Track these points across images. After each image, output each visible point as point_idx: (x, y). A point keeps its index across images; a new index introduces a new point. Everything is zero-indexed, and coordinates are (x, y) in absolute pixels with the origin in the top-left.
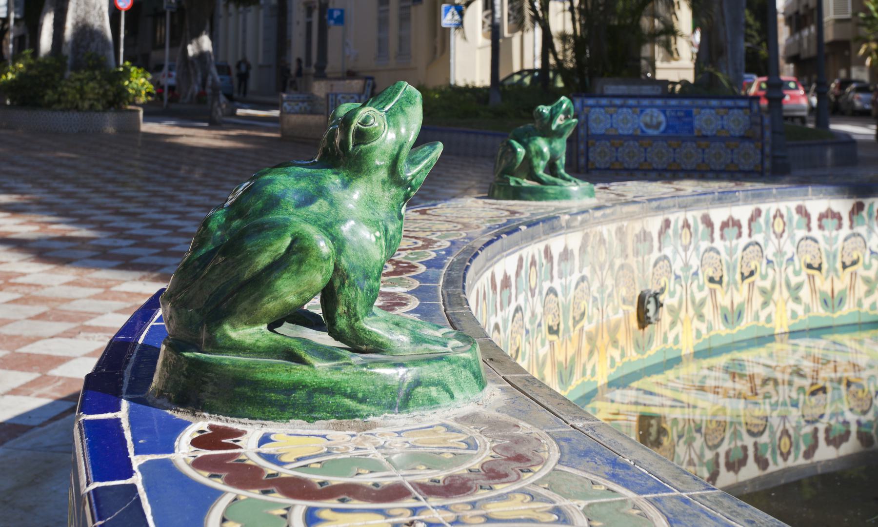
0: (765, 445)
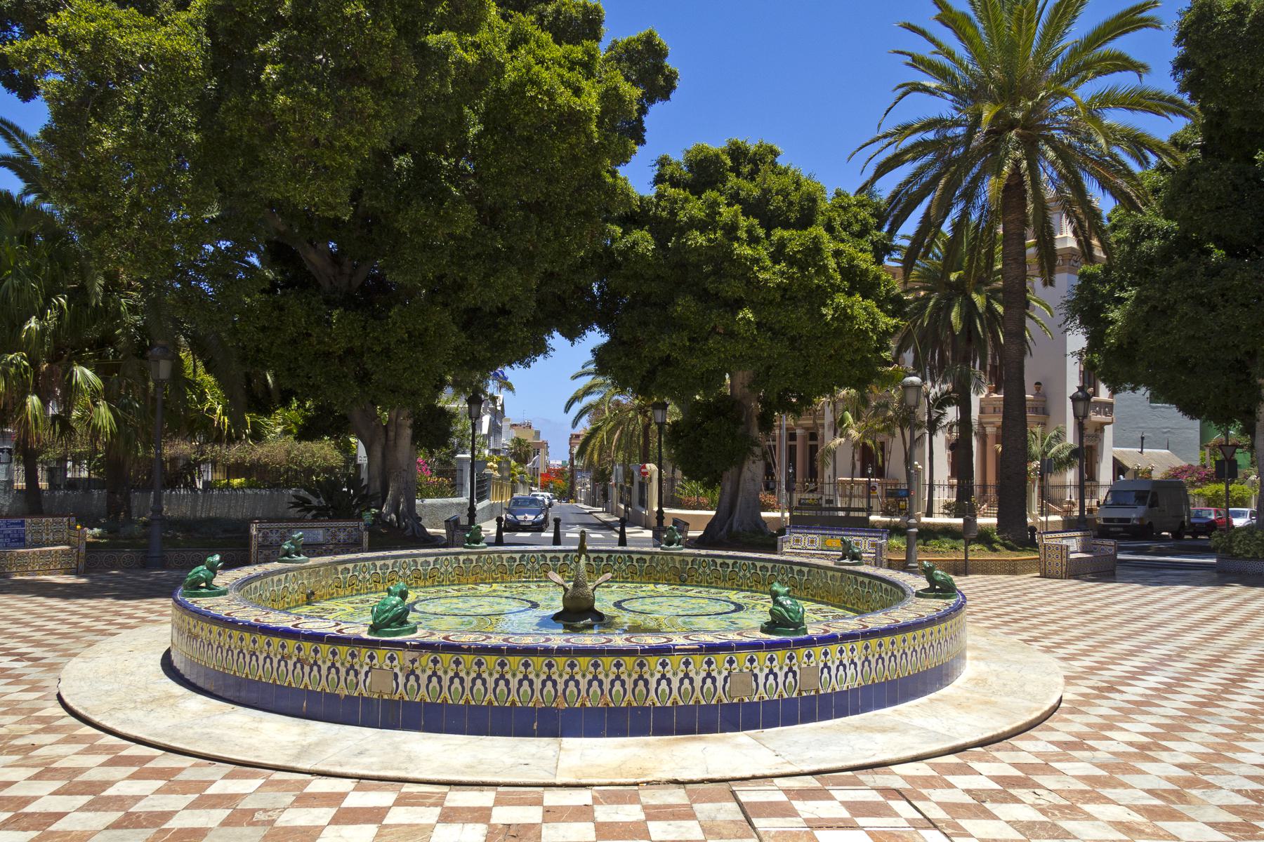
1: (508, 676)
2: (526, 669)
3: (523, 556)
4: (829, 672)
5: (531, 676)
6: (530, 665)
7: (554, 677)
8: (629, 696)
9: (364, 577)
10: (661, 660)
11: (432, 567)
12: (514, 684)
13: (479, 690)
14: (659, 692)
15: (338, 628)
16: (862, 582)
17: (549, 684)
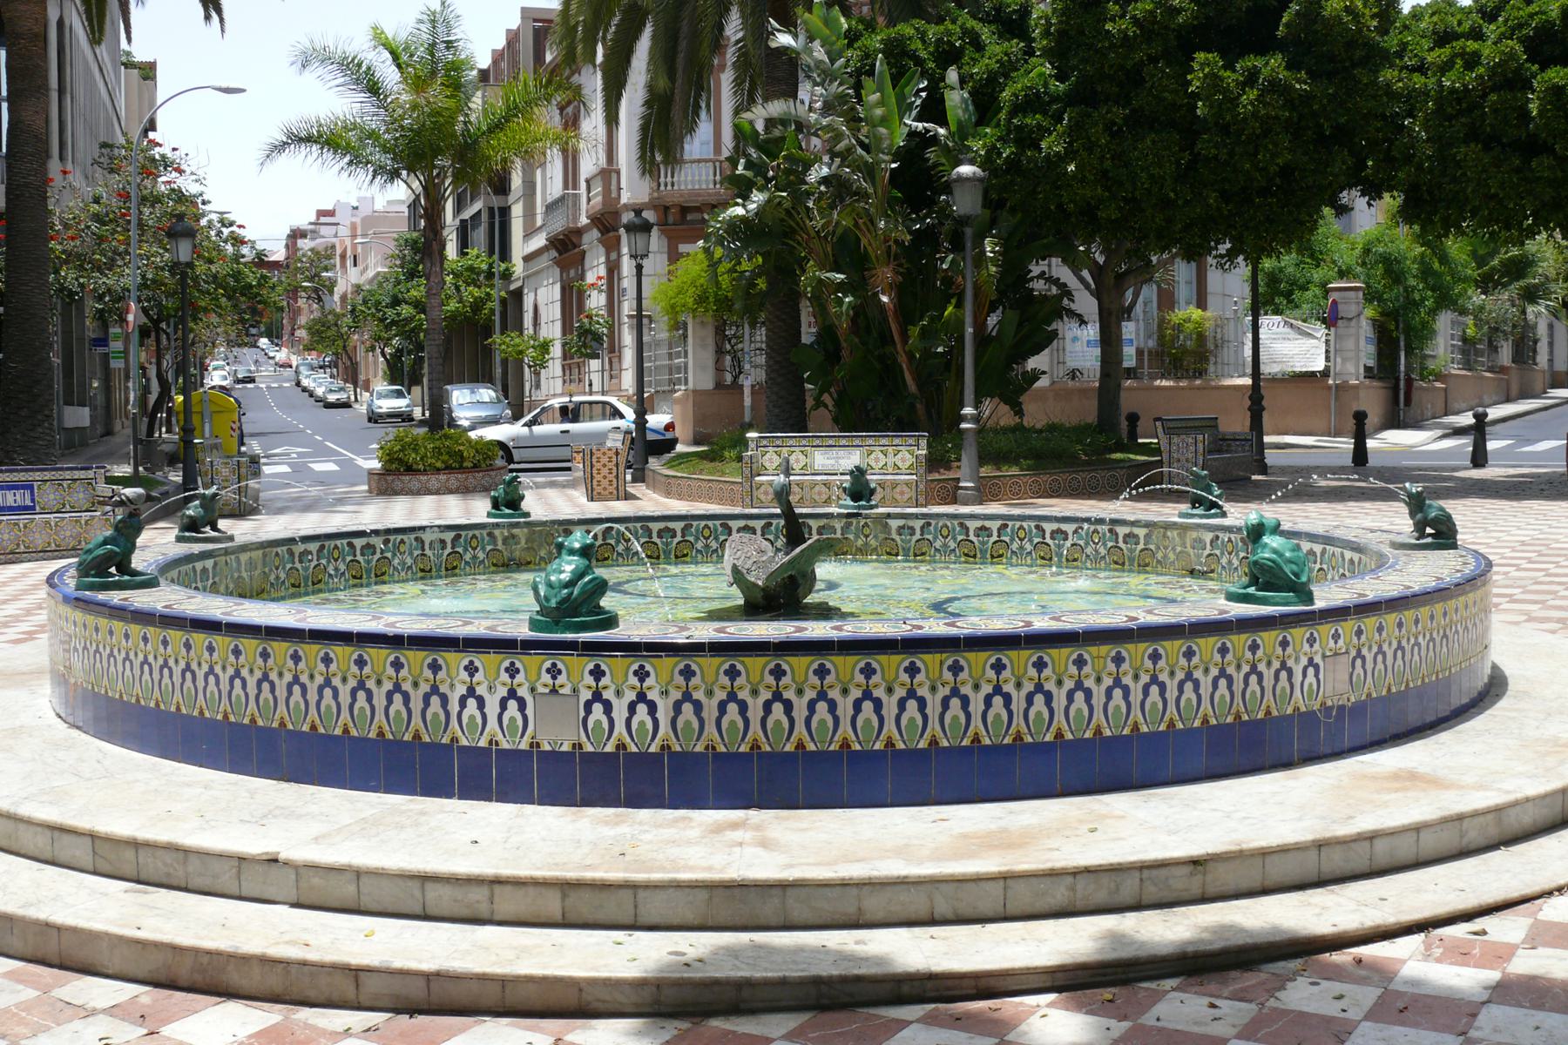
0: (722, 534)
1: (834, 694)
2: (733, 680)
3: (1006, 526)
4: (1230, 686)
5: (741, 695)
6: (694, 674)
7: (920, 693)
8: (845, 729)
9: (475, 557)
10: (635, 667)
11: (995, 538)
12: (845, 707)
13: (822, 722)
14: (990, 719)
17: (998, 701)
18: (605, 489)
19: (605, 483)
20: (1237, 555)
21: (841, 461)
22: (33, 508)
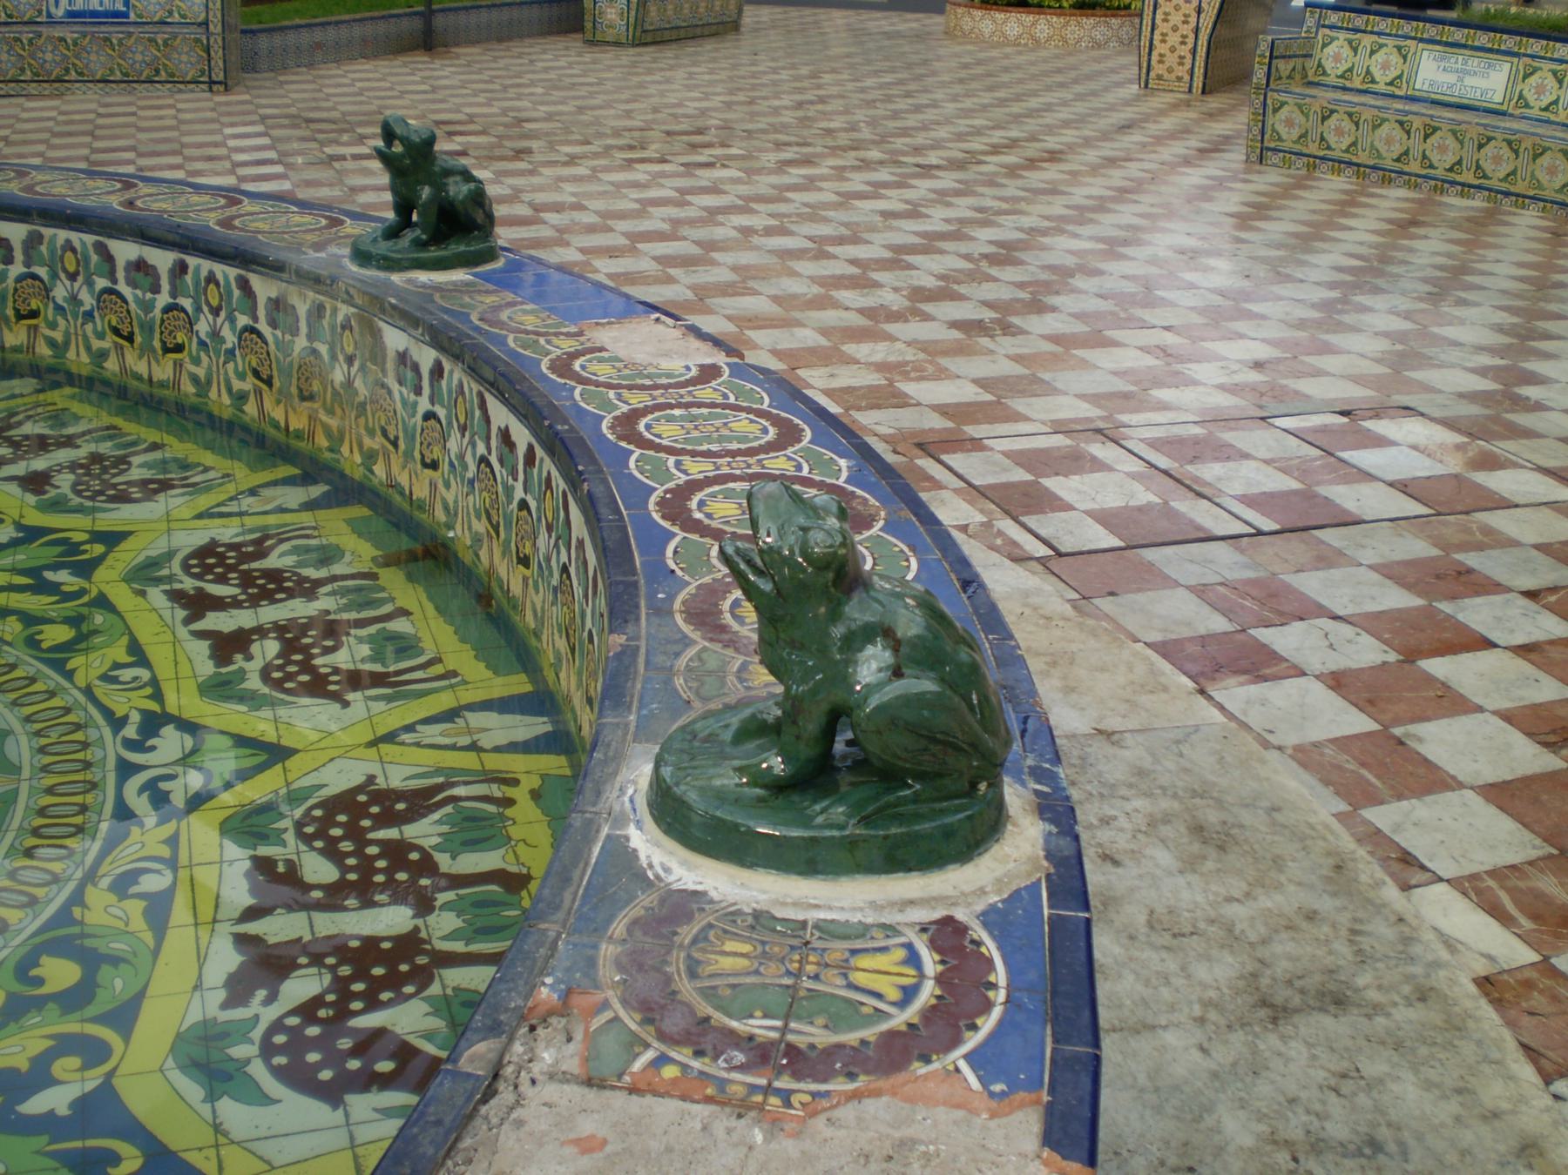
15: (128, 195)
16: (140, 266)
18: (1170, 70)
19: (1171, 60)
20: (89, 283)
21: (1469, 81)
22: (125, 15)
